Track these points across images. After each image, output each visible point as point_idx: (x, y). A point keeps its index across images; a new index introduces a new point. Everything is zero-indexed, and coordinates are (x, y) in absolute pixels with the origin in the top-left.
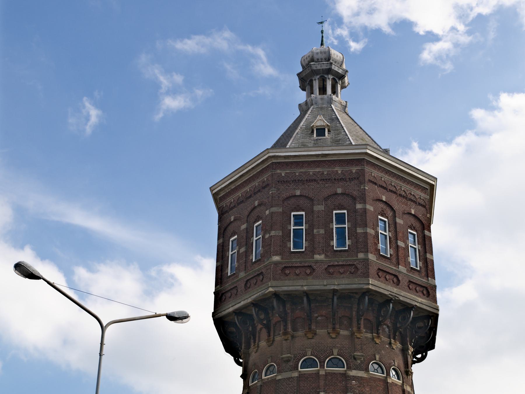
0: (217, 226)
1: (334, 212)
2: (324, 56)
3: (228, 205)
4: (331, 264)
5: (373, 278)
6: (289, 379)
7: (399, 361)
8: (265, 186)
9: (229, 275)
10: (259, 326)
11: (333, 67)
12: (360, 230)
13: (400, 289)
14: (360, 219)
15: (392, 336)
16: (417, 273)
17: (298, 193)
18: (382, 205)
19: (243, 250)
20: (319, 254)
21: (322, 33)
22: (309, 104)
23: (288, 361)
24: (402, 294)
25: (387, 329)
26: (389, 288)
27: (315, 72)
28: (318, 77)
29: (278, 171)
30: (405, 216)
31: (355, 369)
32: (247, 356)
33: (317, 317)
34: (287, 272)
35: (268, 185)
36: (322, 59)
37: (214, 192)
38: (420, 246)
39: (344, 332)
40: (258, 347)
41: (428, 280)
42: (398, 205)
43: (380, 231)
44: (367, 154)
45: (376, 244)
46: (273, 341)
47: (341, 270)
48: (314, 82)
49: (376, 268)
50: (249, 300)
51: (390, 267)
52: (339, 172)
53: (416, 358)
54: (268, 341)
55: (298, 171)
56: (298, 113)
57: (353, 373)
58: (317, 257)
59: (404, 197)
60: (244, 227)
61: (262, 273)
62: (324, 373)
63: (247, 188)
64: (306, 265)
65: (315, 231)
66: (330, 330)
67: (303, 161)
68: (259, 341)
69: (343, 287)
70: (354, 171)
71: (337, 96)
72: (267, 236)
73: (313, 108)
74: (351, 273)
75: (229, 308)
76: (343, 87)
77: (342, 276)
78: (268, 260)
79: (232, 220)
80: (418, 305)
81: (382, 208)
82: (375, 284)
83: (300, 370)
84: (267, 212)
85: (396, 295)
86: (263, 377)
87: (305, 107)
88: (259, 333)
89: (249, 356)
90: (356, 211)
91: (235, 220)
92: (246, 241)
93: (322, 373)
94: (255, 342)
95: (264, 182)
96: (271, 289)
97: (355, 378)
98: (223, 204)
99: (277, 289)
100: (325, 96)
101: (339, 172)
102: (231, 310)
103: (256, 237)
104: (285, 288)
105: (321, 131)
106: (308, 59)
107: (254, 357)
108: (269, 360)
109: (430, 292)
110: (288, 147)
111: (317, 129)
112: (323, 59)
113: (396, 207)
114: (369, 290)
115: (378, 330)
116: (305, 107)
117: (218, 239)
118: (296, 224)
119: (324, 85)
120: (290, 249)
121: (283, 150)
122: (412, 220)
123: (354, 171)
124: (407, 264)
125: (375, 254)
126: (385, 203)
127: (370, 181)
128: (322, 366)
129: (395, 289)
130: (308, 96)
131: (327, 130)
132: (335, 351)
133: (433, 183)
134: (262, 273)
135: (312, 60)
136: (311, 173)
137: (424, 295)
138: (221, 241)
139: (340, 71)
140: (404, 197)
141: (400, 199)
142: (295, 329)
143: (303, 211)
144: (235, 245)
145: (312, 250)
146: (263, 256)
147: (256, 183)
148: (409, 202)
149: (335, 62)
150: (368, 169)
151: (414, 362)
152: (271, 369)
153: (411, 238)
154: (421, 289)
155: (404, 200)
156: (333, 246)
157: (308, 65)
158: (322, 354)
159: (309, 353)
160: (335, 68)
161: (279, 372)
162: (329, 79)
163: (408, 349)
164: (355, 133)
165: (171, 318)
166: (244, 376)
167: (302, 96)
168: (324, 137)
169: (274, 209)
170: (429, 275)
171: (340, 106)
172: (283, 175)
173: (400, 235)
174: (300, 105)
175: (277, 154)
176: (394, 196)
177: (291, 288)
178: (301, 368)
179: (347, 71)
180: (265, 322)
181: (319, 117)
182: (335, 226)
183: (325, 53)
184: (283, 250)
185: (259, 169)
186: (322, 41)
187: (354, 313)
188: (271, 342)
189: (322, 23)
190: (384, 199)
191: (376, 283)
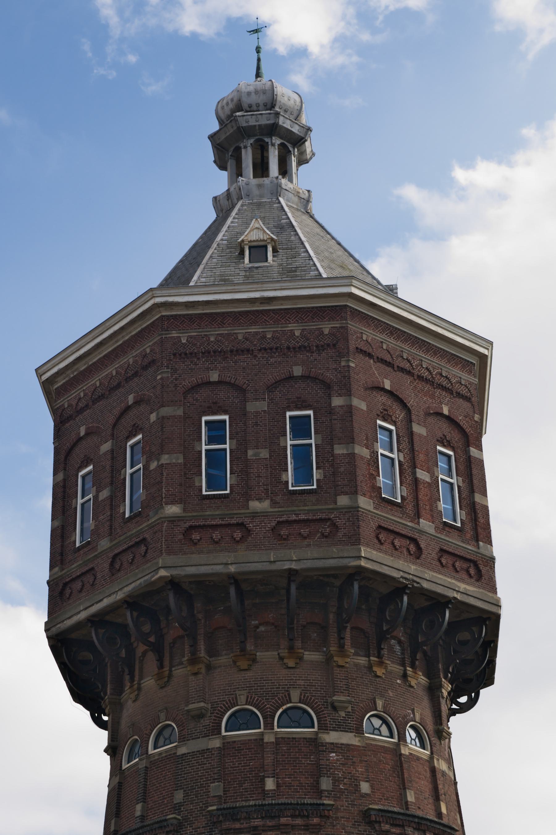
0: (52, 447)
1: (288, 414)
2: (262, 99)
3: (74, 403)
4: (284, 518)
5: (368, 545)
6: (202, 752)
7: (422, 712)
8: (148, 364)
10: (141, 648)
12: (339, 450)
13: (422, 565)
14: (340, 428)
15: (408, 661)
16: (456, 533)
17: (214, 377)
18: (382, 399)
19: (105, 494)
20: (260, 499)
22: (234, 196)
23: (200, 716)
24: (426, 576)
25: (398, 648)
26: (400, 564)
27: (245, 132)
28: (252, 141)
29: (174, 334)
30: (430, 420)
31: (334, 730)
32: (117, 710)
33: (257, 627)
34: (196, 536)
35: (153, 362)
36: (258, 105)
37: (44, 377)
39: (310, 656)
40: (139, 689)
43: (381, 451)
44: (351, 296)
46: (170, 676)
47: (305, 531)
48: (243, 151)
49: (373, 525)
50: (120, 596)
51: (404, 523)
52: (297, 333)
54: (159, 676)
55: (213, 333)
56: (212, 216)
57: (332, 737)
58: (255, 505)
59: (427, 381)
60: (106, 447)
61: (144, 540)
63: (112, 370)
64: (233, 521)
65: (250, 453)
66: (284, 653)
68: (141, 678)
70: (326, 331)
72: (153, 465)
73: (242, 206)
74: (323, 536)
76: (302, 162)
77: (306, 542)
78: (156, 513)
79: (82, 433)
80: (458, 596)
81: (383, 404)
83: (224, 733)
84: (153, 417)
85: (415, 579)
86: (151, 751)
90: (331, 411)
91: (87, 434)
93: (269, 738)
94: (132, 680)
95: (145, 356)
96: (163, 573)
98: (63, 402)
99: (175, 572)
100: (266, 181)
101: (297, 333)
103: (132, 467)
105: (258, 250)
106: (231, 106)
107: (131, 710)
108: (162, 716)
109: (481, 569)
111: (250, 248)
112: (261, 105)
113: (411, 402)
114: (360, 570)
115: (380, 649)
116: (225, 203)
117: (55, 473)
118: (210, 441)
120: (201, 490)
122: (445, 428)
123: (326, 331)
125: (371, 497)
126: (390, 393)
127: (359, 351)
128: (269, 725)
129: (413, 567)
130: (232, 180)
131: (270, 249)
132: (295, 695)
133: (486, 352)
134: (144, 540)
135: (239, 107)
136: (240, 337)
137: (470, 576)
138: (61, 476)
139: (295, 129)
140: (427, 381)
141: (421, 385)
142: (212, 652)
143: (225, 412)
144: (89, 485)
145: (244, 492)
146: (145, 505)
147: (129, 359)
148: (438, 392)
149: (286, 111)
150: (354, 326)
151: (453, 713)
152: (166, 733)
154: (465, 565)
155: (427, 387)
156: (287, 482)
159: (243, 699)
160: (285, 123)
161: (183, 739)
162: (273, 145)
163: (441, 686)
164: (326, 254)
166: (112, 750)
167: (220, 182)
168: (266, 264)
169: (166, 411)
170: (481, 537)
171: (296, 199)
172: (184, 341)
174: (215, 198)
175: (171, 299)
176: (408, 379)
178: (226, 731)
179: (309, 129)
180: (152, 639)
181: (254, 224)
182: (289, 443)
183: (264, 92)
184: (186, 493)
186: (258, 68)
187: (331, 616)
188: (164, 680)
191: (375, 554)
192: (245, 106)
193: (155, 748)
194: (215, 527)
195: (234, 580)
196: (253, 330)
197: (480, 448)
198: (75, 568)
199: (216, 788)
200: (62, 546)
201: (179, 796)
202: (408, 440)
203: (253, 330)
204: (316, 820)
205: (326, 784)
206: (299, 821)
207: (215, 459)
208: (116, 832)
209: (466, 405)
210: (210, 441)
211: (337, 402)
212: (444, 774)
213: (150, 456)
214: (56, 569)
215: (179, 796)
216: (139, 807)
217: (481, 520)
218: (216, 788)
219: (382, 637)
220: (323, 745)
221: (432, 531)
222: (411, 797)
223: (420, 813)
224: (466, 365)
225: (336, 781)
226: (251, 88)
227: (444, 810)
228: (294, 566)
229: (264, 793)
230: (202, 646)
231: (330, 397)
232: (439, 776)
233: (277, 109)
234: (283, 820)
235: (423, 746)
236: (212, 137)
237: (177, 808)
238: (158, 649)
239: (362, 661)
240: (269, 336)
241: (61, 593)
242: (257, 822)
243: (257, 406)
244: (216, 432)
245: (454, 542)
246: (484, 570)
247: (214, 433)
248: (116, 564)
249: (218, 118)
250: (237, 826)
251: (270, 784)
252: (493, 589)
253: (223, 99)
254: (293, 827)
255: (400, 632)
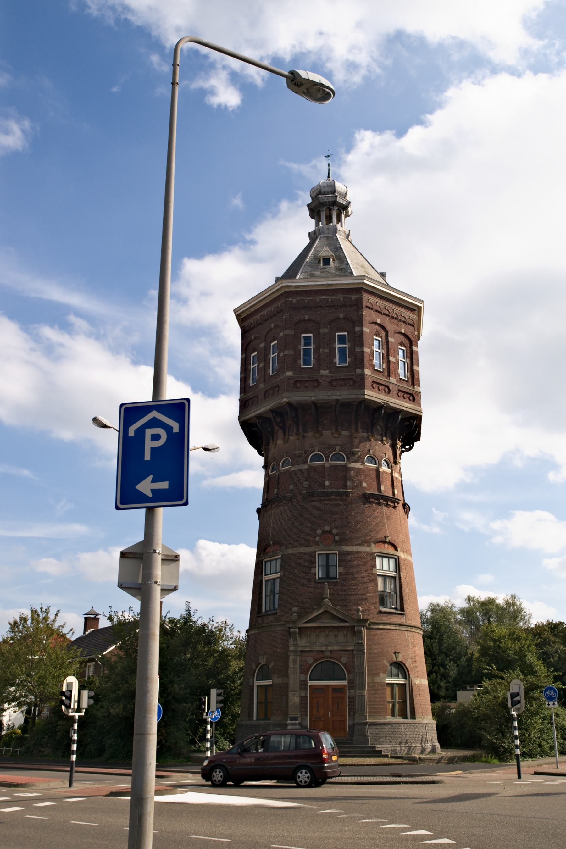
0: (240, 343)
1: (337, 334)
2: (330, 189)
3: (249, 325)
4: (334, 378)
5: (368, 389)
6: (301, 470)
7: (389, 454)
8: (279, 311)
9: (251, 385)
10: (276, 428)
11: (338, 199)
12: (358, 349)
13: (390, 397)
14: (358, 340)
15: (384, 434)
16: (405, 382)
17: (307, 318)
19: (262, 365)
20: (325, 370)
21: (329, 166)
22: (317, 233)
23: (300, 456)
25: (380, 429)
27: (322, 204)
28: (325, 208)
29: (290, 299)
30: (396, 335)
31: (353, 462)
32: (267, 451)
33: (323, 421)
34: (298, 385)
35: (282, 311)
36: (328, 192)
37: (237, 313)
38: (408, 360)
39: (344, 433)
40: (276, 444)
41: (414, 388)
42: (391, 326)
43: (375, 349)
44: (364, 284)
45: (371, 361)
46: (288, 440)
47: (342, 383)
48: (321, 213)
49: (371, 381)
50: (268, 408)
51: (382, 379)
52: (341, 299)
53: (405, 448)
54: (284, 439)
55: (306, 299)
56: (308, 241)
57: (353, 465)
58: (323, 372)
59: (395, 319)
60: (262, 345)
62: (328, 466)
63: (264, 312)
64: (314, 379)
65: (321, 350)
66: (334, 431)
67: (311, 290)
68: (277, 439)
69: (344, 397)
70: (353, 299)
71: (342, 226)
72: (282, 355)
74: (350, 385)
75: (253, 413)
76: (347, 215)
77: (343, 388)
78: (282, 375)
79: (253, 338)
80: (405, 409)
82: (371, 394)
83: (309, 463)
84: (281, 334)
86: (280, 469)
87: (313, 236)
88: (277, 433)
89: (269, 451)
90: (354, 333)
91: (255, 338)
92: (264, 358)
93: (327, 465)
94: (273, 440)
95: (278, 308)
96: (285, 400)
97: (353, 469)
98: (245, 324)
99: (290, 400)
101: (341, 299)
102: (253, 414)
104: (297, 399)
105: (327, 261)
106: (317, 192)
107: (273, 451)
108: (285, 455)
109: (414, 397)
110: (298, 277)
111: (323, 259)
113: (388, 328)
115: (372, 430)
116: (313, 236)
117: (242, 354)
118: (305, 345)
119: (330, 213)
121: (294, 281)
122: (402, 338)
123: (353, 299)
124: (397, 375)
125: (370, 369)
126: (380, 325)
127: (367, 307)
128: (327, 460)
129: (386, 397)
130: (317, 224)
131: (332, 260)
132: (338, 448)
134: (278, 385)
135: (320, 193)
136: (318, 301)
137: (410, 400)
138: (244, 356)
139: (344, 203)
140: (395, 319)
141: (393, 320)
142: (305, 431)
143: (311, 333)
144: (255, 360)
146: (278, 371)
147: (272, 308)
148: (400, 323)
149: (340, 194)
150: (365, 296)
151: (403, 452)
152: (287, 462)
153: (401, 353)
154: (408, 396)
155: (396, 321)
157: (316, 197)
158: (327, 450)
159: (317, 450)
160: (339, 200)
161: (293, 465)
163: (397, 444)
164: (356, 261)
165: (205, 449)
166: (266, 467)
167: (311, 225)
169: (287, 332)
170: (415, 384)
171: (344, 234)
173: (391, 351)
174: (309, 233)
175: (289, 284)
176: (387, 318)
177: (301, 398)
179: (350, 203)
180: (281, 425)
181: (325, 249)
182: (337, 346)
183: (331, 186)
184: (295, 366)
185: (271, 298)
187: (353, 417)
188: (286, 441)
189: (328, 156)
190: (379, 321)
192: (323, 192)
193: (282, 467)
194: (306, 381)
195: (314, 403)
196: (323, 298)
197: (417, 346)
198: (250, 395)
199: (306, 484)
200: (245, 385)
201: (291, 487)
202: (386, 345)
203: (323, 298)
204: (345, 497)
205: (349, 483)
206: (338, 498)
207: (307, 352)
208: (267, 499)
209: (412, 328)
210: (305, 345)
211: (357, 329)
212: (397, 478)
213: (280, 351)
214: (242, 394)
215: (291, 487)
216: (276, 490)
217: (416, 377)
218: (306, 484)
219: (373, 425)
220: (348, 468)
221: (395, 382)
222: (383, 488)
223: (386, 494)
224: (412, 310)
225: (353, 482)
226: (325, 184)
227: (396, 492)
228: (338, 398)
229: (325, 487)
230: (301, 428)
231: (354, 327)
232: (394, 479)
233: (336, 194)
234: (332, 497)
235: (389, 468)
236: (308, 206)
237: (290, 492)
238: (283, 429)
239: (365, 435)
240: (330, 300)
241: (265, 550)
242: (322, 498)
243: (324, 330)
244: (307, 341)
245: (405, 387)
246: (416, 397)
247: (307, 341)
248: (266, 395)
249: (311, 197)
250: (314, 499)
251: (327, 483)
252: (420, 405)
253: (313, 188)
254: (336, 500)
255: (381, 423)
